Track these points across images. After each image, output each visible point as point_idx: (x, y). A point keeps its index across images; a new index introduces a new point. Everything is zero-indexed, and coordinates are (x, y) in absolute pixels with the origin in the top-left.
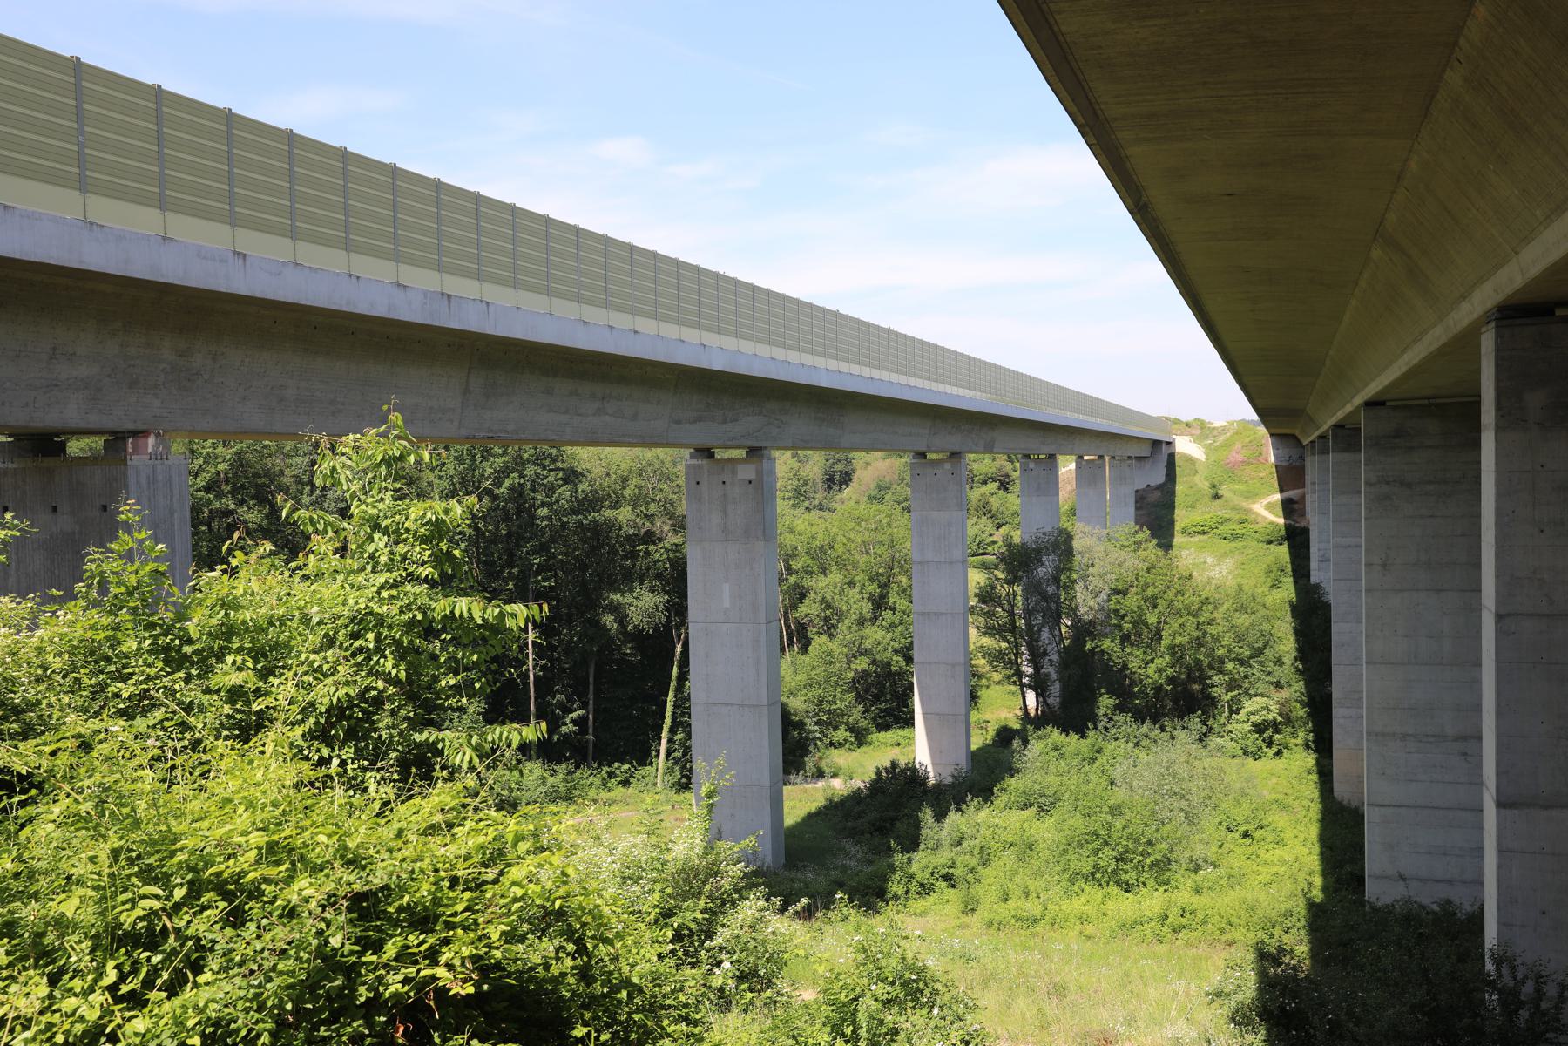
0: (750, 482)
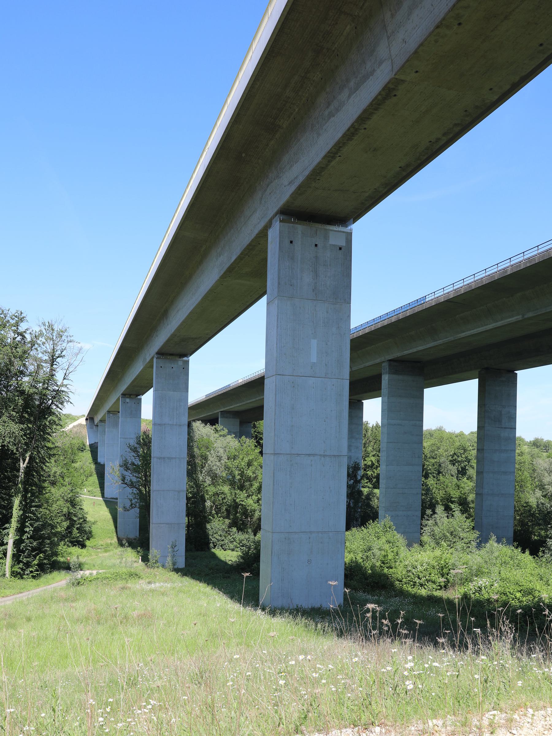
0: (340, 249)
